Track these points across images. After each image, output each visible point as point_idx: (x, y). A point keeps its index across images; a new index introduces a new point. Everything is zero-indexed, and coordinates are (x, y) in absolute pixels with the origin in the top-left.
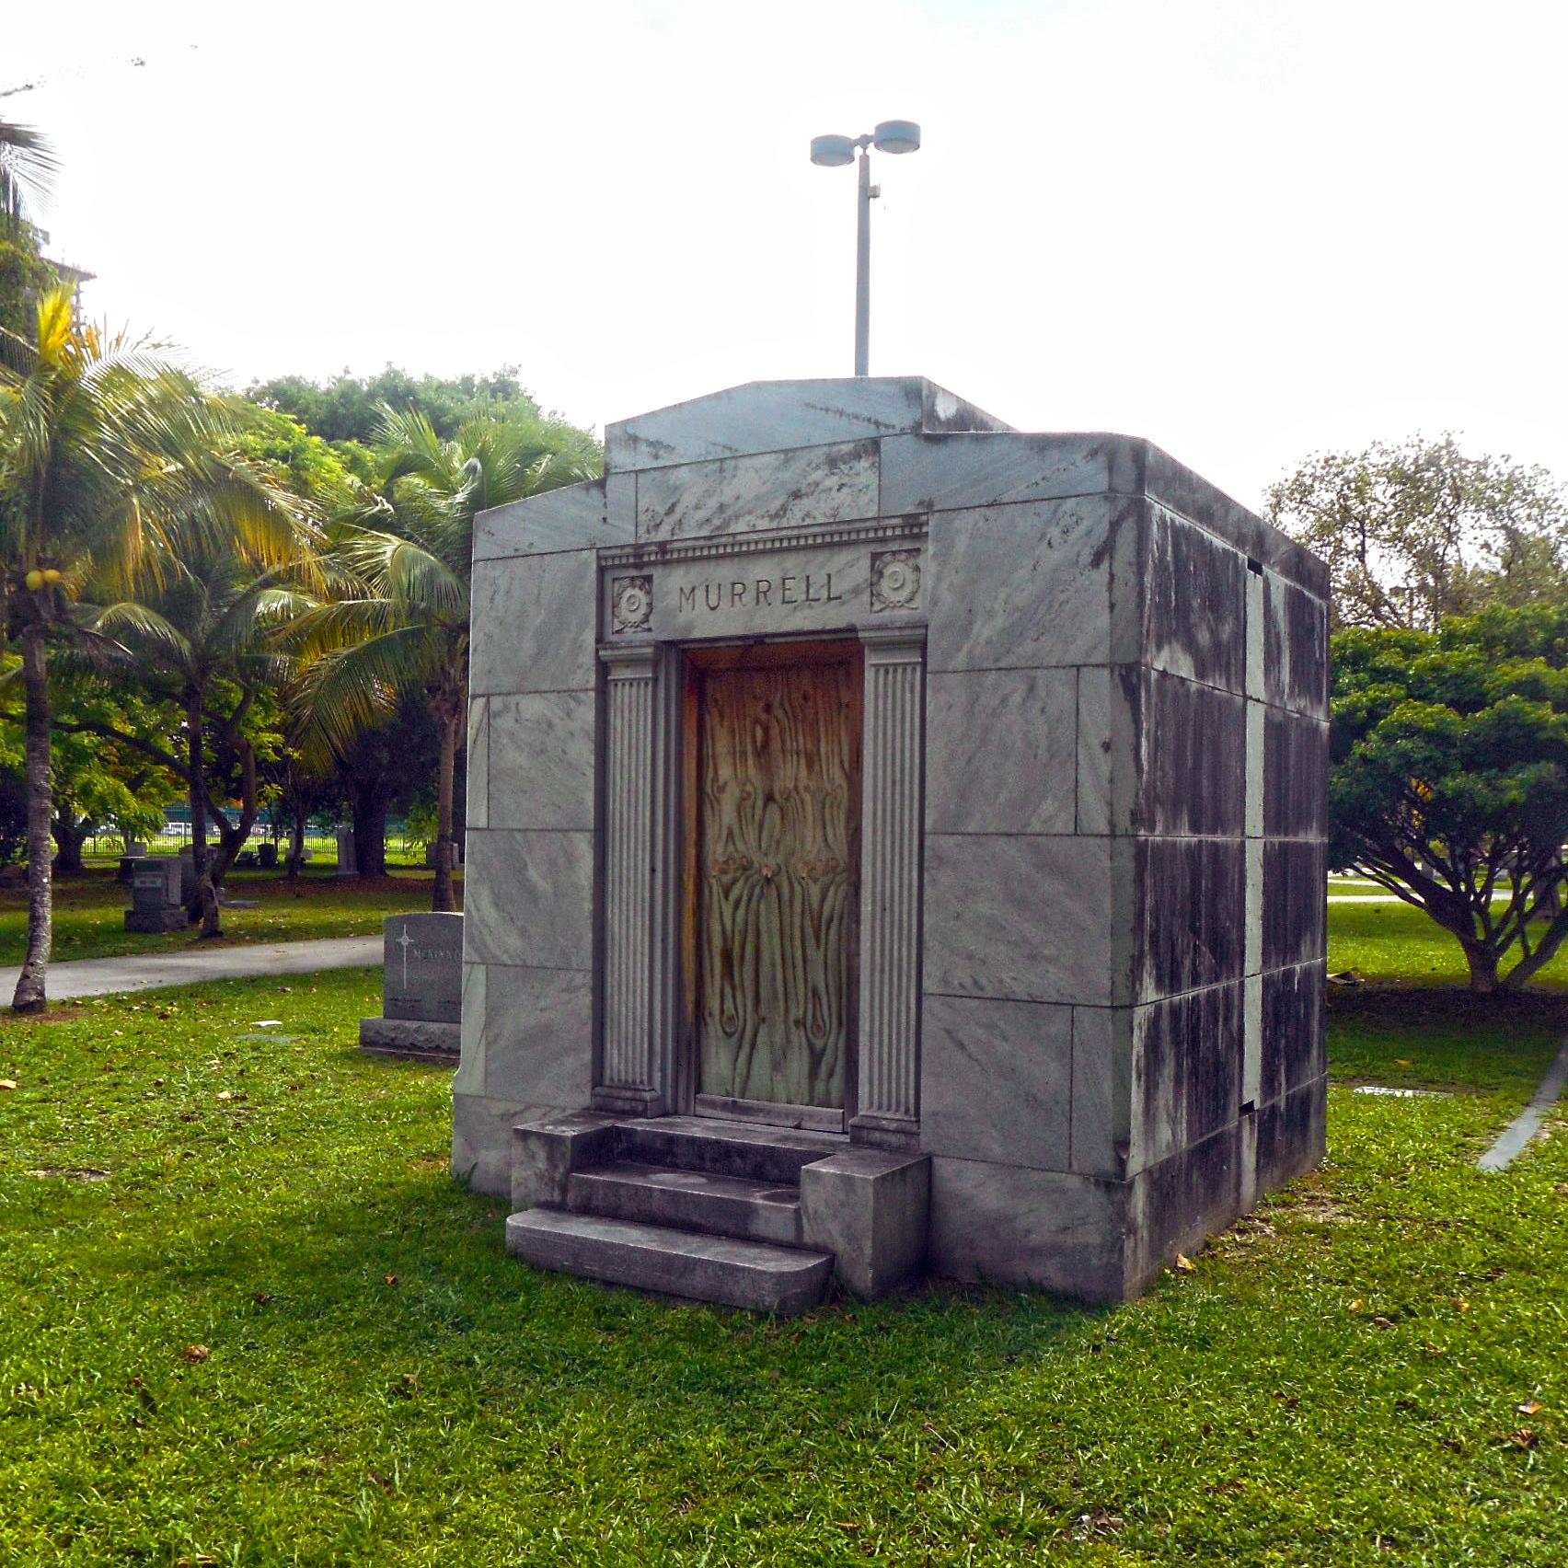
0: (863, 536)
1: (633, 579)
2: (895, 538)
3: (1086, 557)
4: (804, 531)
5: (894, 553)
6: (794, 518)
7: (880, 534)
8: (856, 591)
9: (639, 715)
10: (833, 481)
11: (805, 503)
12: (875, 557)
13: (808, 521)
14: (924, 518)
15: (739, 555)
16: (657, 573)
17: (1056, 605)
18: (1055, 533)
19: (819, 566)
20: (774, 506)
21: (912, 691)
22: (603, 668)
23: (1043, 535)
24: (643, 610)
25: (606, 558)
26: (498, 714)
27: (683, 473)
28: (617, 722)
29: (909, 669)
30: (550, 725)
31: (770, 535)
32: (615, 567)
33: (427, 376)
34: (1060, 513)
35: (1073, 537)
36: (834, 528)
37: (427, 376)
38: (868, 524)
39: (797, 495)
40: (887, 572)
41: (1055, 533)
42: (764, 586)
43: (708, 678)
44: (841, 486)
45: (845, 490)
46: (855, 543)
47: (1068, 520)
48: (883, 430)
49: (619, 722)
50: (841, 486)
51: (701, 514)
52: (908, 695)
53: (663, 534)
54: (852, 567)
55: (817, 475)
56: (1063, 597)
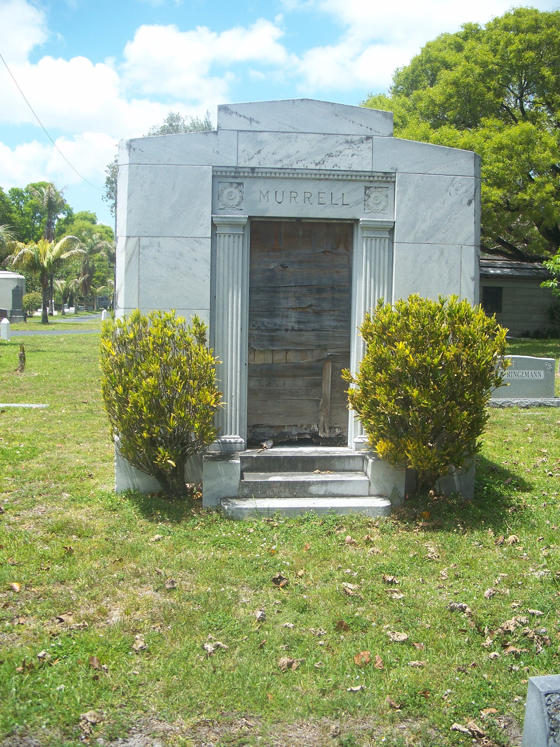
0: (363, 178)
1: (231, 183)
2: (376, 181)
3: (465, 201)
4: (333, 172)
5: (376, 188)
6: (328, 165)
7: (371, 179)
8: (357, 203)
9: (236, 253)
10: (350, 152)
11: (335, 160)
12: (367, 188)
13: (336, 168)
14: (393, 175)
15: (295, 179)
16: (246, 182)
17: (453, 220)
18: (452, 190)
19: (338, 190)
20: (318, 159)
21: (384, 250)
22: (214, 226)
23: (447, 190)
24: (238, 199)
25: (217, 172)
26: (145, 247)
27: (265, 136)
28: (220, 255)
29: (383, 240)
30: (181, 254)
31: (346, 173)
32: (219, 176)
33: (462, 27)
34: (454, 181)
35: (460, 192)
36: (349, 173)
37: (462, 27)
38: (367, 174)
39: (330, 155)
40: (372, 196)
41: (452, 190)
42: (308, 195)
43: (265, 233)
44: (353, 155)
45: (355, 156)
46: (358, 181)
47: (458, 185)
48: (374, 133)
49: (222, 254)
50: (353, 155)
51: (277, 157)
52: (382, 252)
53: (253, 164)
54: (354, 193)
55: (341, 148)
56: (456, 216)
